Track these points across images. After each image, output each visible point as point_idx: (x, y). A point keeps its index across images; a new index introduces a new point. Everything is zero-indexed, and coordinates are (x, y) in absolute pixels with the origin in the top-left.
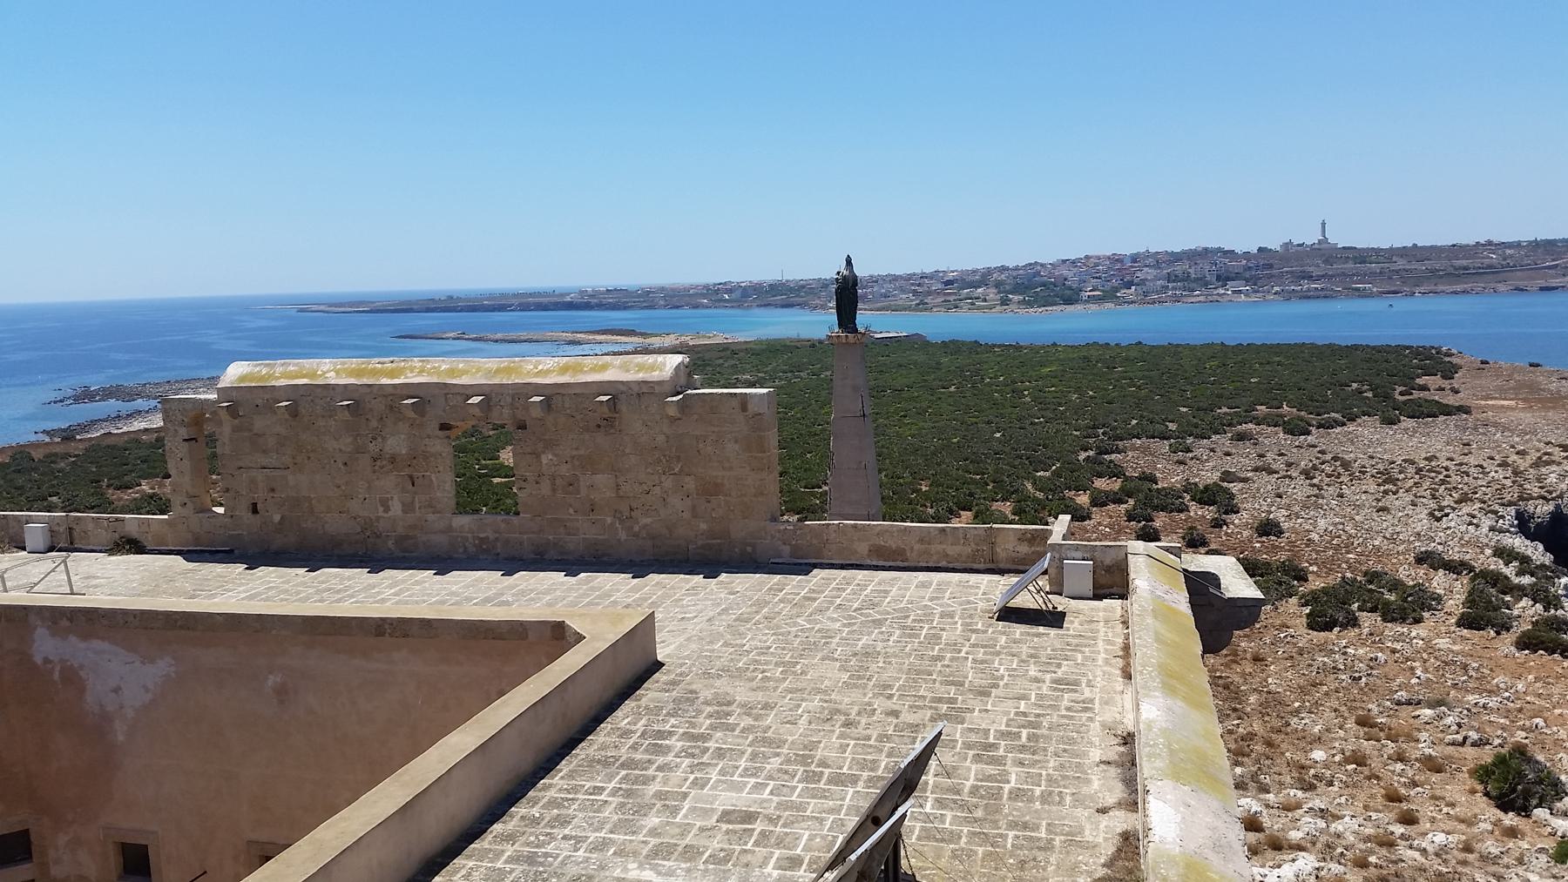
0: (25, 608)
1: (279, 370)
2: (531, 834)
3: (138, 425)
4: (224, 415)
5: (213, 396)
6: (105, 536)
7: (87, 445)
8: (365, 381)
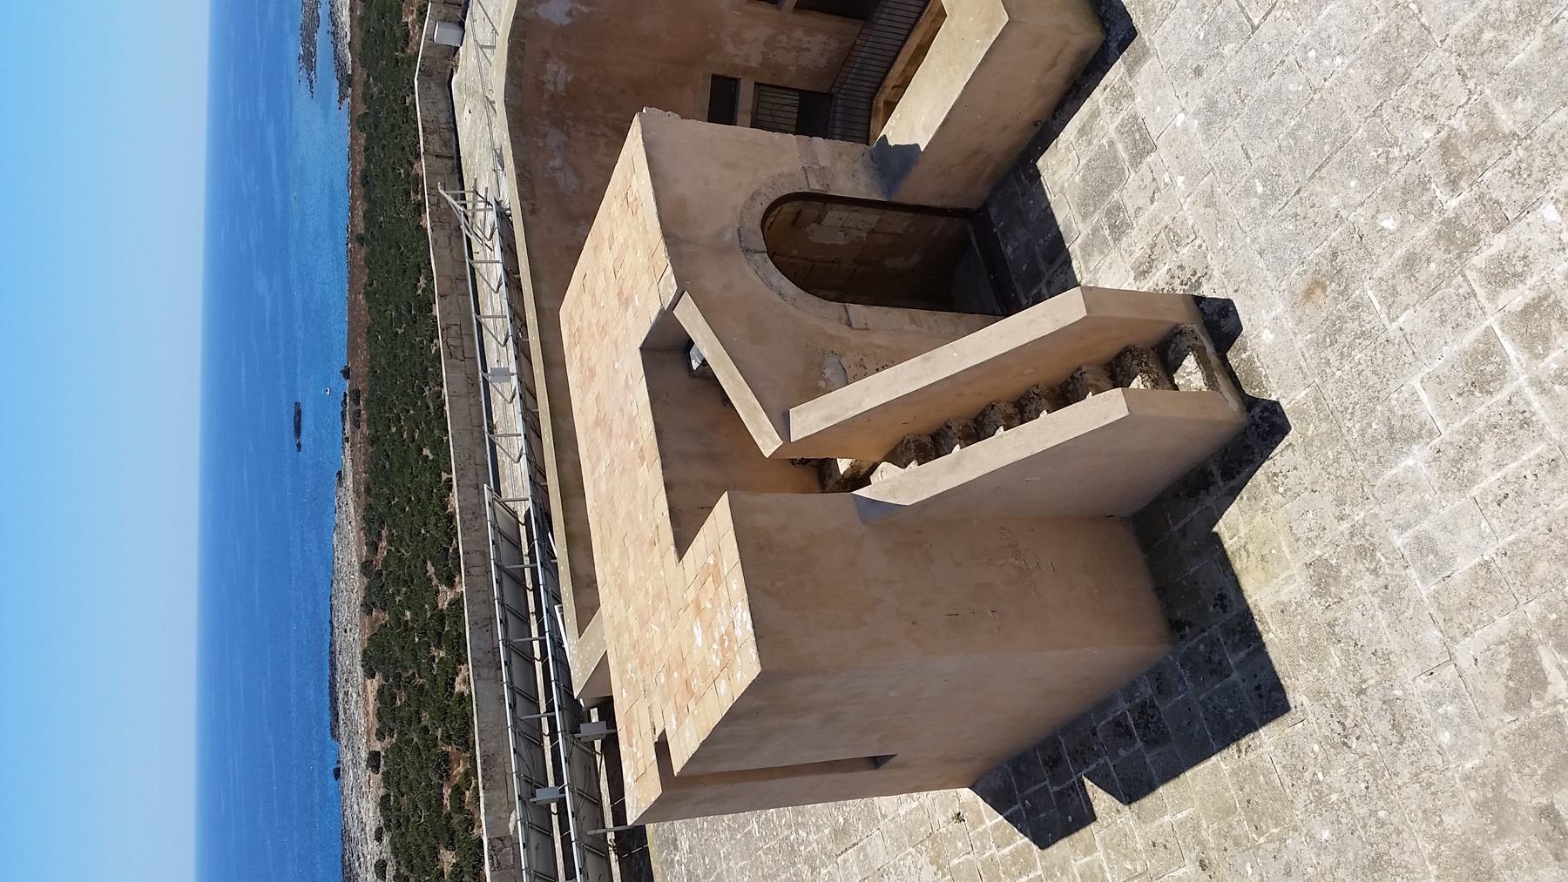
0: (516, 18)
3: (345, 17)
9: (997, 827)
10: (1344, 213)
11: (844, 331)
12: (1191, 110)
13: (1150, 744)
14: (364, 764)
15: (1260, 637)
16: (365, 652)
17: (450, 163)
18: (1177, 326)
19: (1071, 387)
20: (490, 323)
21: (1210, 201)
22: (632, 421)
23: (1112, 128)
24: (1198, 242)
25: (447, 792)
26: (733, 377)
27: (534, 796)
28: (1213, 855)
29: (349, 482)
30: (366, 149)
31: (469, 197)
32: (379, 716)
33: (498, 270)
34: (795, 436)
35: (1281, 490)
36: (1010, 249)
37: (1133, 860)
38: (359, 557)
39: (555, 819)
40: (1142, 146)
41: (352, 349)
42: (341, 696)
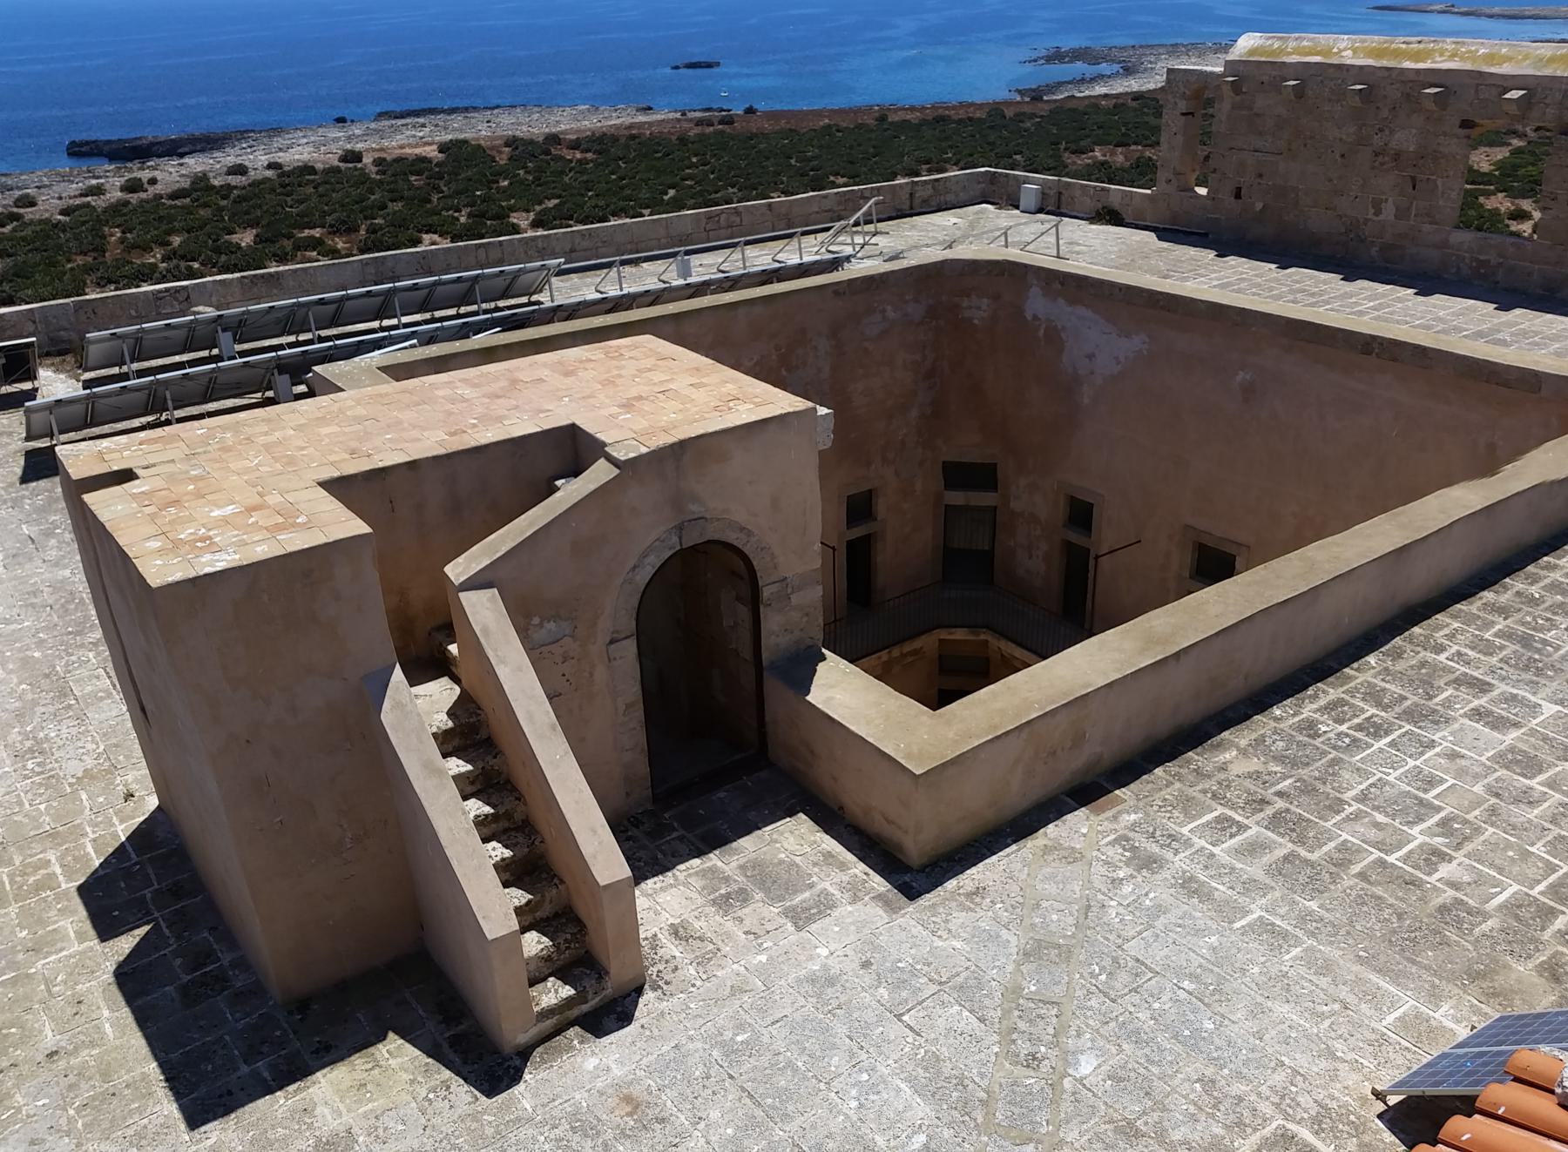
0: (1026, 266)
1: (1292, 44)
2: (1528, 613)
3: (1100, 90)
4: (1226, 90)
5: (1219, 69)
6: (1090, 204)
7: (1053, 106)
8: (1385, 63)
9: (115, 835)
10: (702, 1125)
11: (602, 638)
12: (829, 962)
13: (184, 990)
14: (349, 147)
15: (280, 1089)
16: (465, 142)
17: (906, 206)
18: (607, 973)
19: (544, 875)
20: (737, 255)
21: (736, 991)
22: (500, 419)
23: (827, 885)
24: (698, 983)
25: (317, 232)
26: (530, 525)
27: (224, 330)
28: (62, 1064)
29: (642, 118)
30: (970, 119)
31: (870, 228)
32: (399, 160)
33: (794, 260)
34: (462, 595)
35: (431, 1096)
36: (722, 795)
37: (65, 982)
38: (565, 132)
39: (205, 353)
40: (800, 918)
41: (773, 115)
42: (421, 120)
